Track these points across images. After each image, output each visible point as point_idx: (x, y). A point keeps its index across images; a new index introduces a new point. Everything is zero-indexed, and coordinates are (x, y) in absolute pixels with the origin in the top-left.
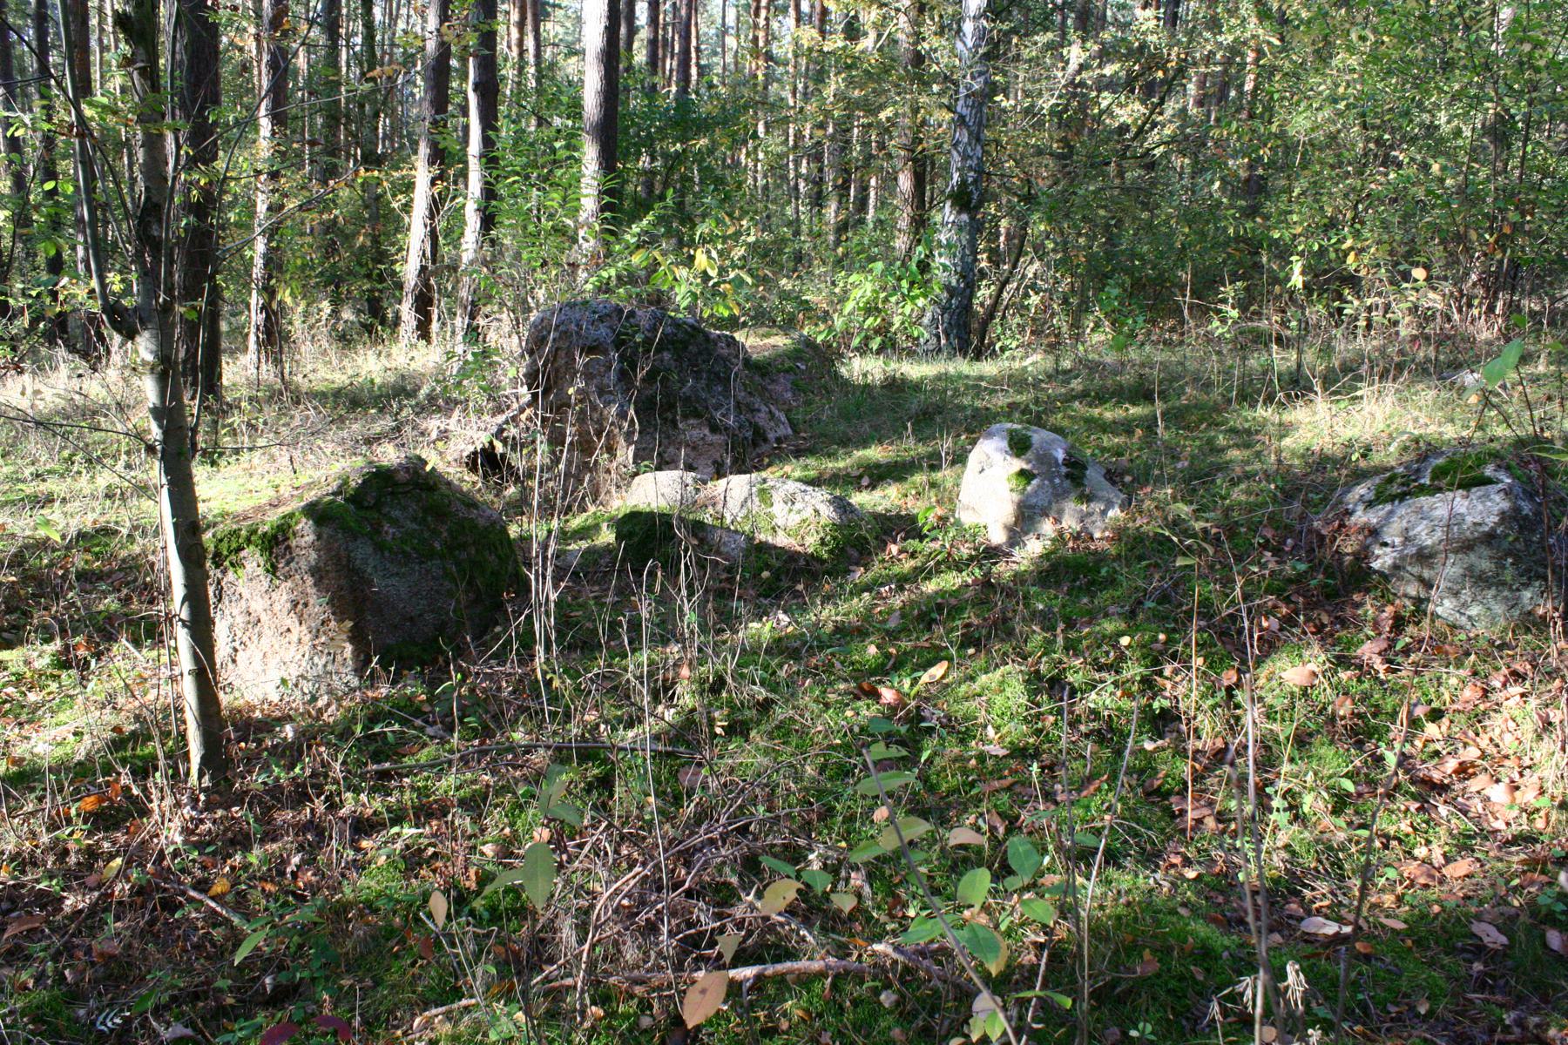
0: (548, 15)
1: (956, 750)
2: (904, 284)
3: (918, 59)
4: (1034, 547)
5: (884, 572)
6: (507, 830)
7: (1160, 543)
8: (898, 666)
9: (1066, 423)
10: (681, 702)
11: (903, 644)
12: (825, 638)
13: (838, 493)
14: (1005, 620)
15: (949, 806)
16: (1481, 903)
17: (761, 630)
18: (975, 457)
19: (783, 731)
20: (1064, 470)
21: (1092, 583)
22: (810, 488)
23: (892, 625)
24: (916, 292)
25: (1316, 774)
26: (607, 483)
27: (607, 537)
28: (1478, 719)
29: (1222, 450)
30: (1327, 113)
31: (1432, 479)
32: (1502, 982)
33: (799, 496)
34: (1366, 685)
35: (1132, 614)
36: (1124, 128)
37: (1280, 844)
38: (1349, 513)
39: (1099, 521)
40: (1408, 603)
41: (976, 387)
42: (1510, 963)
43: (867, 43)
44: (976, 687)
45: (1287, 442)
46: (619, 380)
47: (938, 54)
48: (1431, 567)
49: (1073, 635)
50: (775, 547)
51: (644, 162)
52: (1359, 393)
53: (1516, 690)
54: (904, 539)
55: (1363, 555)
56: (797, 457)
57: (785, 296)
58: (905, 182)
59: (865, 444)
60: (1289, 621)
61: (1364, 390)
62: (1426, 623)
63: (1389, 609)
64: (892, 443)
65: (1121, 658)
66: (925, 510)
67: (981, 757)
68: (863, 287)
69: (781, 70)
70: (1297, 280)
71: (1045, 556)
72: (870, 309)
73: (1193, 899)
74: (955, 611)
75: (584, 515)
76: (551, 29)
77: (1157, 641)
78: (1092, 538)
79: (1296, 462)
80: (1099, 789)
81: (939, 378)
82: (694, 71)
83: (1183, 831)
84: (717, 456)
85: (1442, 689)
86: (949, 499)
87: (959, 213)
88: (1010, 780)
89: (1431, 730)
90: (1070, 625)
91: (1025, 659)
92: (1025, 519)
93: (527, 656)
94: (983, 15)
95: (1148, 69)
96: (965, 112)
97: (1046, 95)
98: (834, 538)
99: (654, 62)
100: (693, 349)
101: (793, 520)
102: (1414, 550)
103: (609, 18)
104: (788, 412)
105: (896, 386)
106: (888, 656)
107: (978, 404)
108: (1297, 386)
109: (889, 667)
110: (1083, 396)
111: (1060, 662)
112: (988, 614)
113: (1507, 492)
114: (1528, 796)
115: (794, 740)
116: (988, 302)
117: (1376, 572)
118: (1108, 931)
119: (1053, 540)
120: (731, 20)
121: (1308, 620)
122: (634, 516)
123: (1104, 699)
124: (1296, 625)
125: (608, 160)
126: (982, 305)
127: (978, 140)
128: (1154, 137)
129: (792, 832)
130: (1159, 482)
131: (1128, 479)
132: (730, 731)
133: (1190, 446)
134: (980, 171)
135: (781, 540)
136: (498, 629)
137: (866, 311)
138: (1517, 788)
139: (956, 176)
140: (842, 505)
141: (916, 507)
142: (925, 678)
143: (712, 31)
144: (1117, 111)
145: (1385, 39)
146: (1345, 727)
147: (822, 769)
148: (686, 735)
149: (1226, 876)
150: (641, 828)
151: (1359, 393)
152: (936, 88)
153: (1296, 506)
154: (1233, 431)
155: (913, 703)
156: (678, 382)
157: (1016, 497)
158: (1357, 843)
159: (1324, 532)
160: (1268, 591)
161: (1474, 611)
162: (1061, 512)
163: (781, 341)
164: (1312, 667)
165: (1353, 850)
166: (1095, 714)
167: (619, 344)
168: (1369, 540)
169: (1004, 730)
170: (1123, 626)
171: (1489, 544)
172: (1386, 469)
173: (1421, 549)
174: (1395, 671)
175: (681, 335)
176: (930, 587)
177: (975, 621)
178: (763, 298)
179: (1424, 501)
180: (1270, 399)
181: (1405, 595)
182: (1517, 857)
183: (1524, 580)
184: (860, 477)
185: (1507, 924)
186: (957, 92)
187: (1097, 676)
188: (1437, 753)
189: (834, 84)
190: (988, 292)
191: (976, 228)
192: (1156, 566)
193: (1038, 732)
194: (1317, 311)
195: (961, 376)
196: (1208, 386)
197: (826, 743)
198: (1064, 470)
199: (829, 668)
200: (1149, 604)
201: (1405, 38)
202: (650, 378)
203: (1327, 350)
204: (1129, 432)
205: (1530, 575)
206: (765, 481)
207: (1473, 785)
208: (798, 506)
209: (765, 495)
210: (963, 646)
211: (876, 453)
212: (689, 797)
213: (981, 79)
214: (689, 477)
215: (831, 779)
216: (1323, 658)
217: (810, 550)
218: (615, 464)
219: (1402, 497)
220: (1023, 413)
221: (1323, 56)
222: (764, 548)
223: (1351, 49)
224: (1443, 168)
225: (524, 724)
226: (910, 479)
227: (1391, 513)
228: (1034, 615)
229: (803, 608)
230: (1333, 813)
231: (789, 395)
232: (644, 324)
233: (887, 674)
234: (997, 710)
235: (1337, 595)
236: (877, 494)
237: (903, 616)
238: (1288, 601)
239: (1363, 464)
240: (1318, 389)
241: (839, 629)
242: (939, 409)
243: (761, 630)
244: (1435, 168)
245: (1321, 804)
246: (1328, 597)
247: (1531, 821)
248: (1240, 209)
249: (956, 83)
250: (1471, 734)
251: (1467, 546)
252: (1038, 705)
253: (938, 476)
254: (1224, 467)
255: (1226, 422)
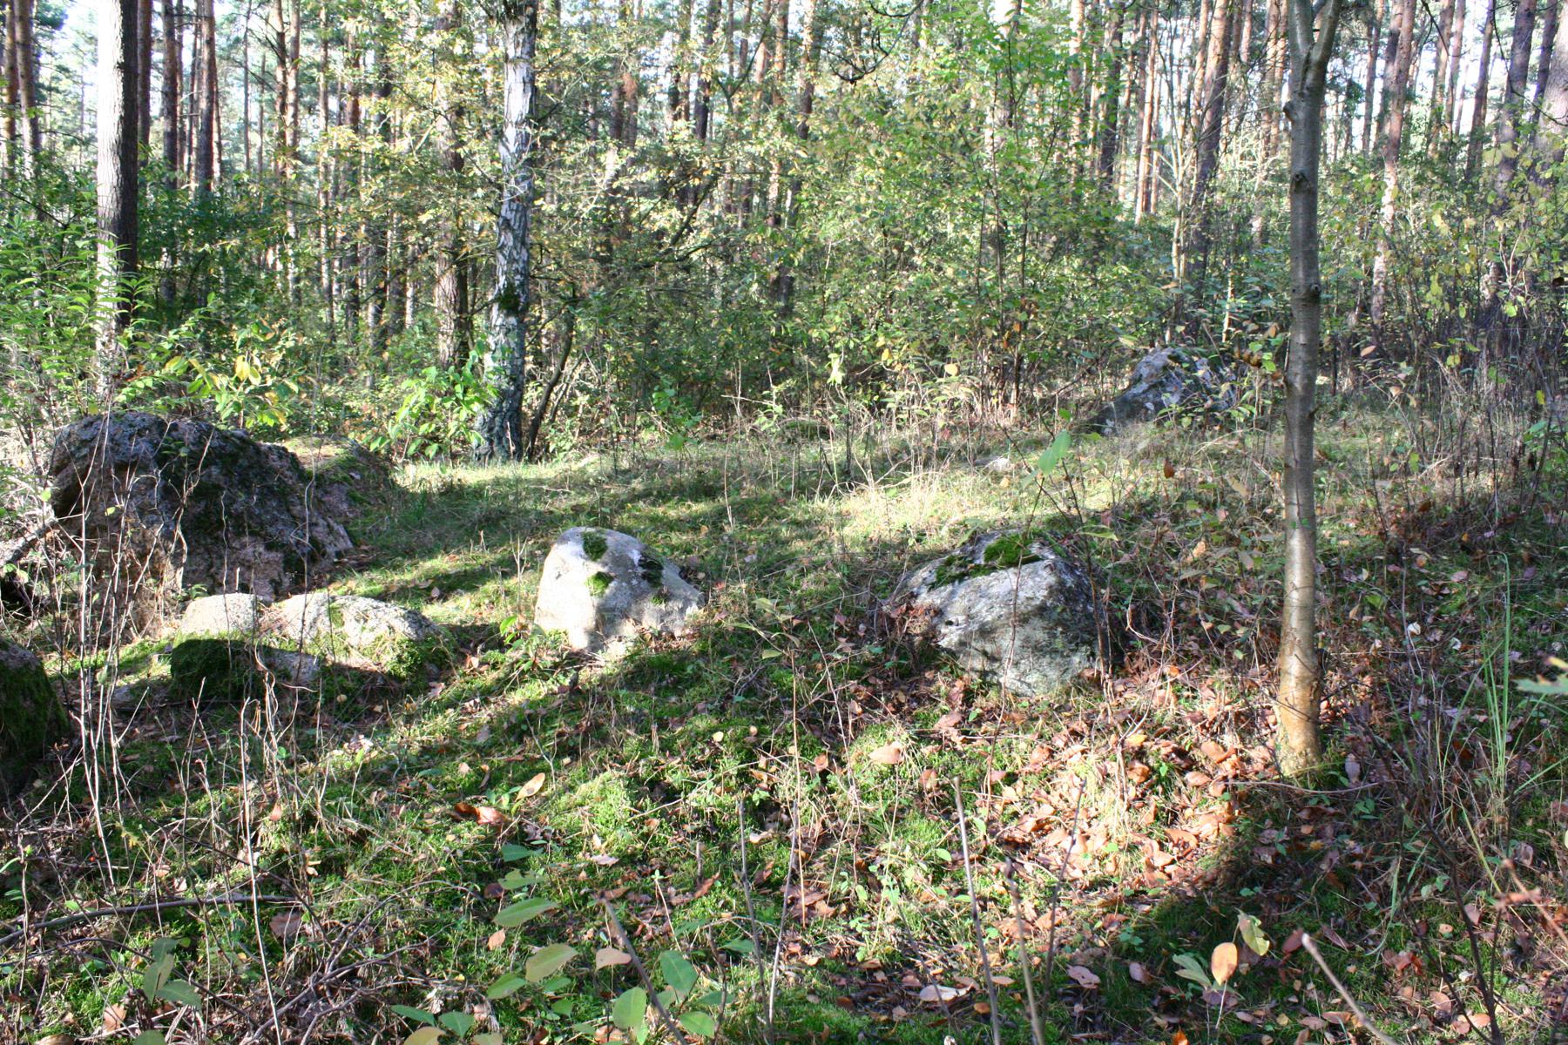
0: (44, 98)
1: (564, 864)
2: (459, 389)
3: (458, 162)
4: (615, 653)
5: (467, 687)
6: (70, 1017)
7: (740, 637)
8: (493, 783)
9: (631, 523)
10: (265, 844)
11: (495, 760)
12: (413, 760)
13: (409, 606)
14: (599, 726)
15: (564, 923)
16: (1073, 948)
17: (336, 759)
18: (552, 562)
19: (382, 863)
20: (640, 571)
21: (678, 681)
22: (382, 604)
23: (481, 740)
24: (470, 396)
25: (913, 848)
26: (155, 609)
27: (160, 669)
28: (1047, 777)
29: (786, 542)
30: (854, 220)
31: (986, 560)
32: (1100, 1018)
33: (371, 613)
34: (947, 758)
35: (723, 709)
36: (662, 233)
37: (889, 919)
38: (914, 596)
39: (677, 620)
40: (975, 676)
41: (538, 489)
42: (1104, 999)
43: (401, 146)
44: (577, 797)
45: (847, 531)
46: (163, 498)
47: (476, 158)
48: (993, 641)
49: (666, 735)
50: (350, 668)
51: (164, 262)
52: (905, 481)
53: (1077, 747)
54: (484, 651)
55: (931, 635)
56: (360, 571)
57: (327, 403)
58: (447, 285)
59: (431, 554)
60: (870, 703)
61: (910, 478)
62: (992, 694)
63: (959, 683)
64: (459, 553)
65: (717, 754)
66: (502, 618)
67: (591, 869)
68: (414, 393)
69: (310, 169)
70: (837, 376)
71: (630, 659)
72: (425, 415)
73: (819, 985)
74: (548, 719)
75: (129, 647)
76: (51, 115)
77: (749, 734)
78: (673, 637)
79: (858, 550)
80: (713, 888)
81: (497, 482)
82: (216, 167)
83: (798, 919)
84: (275, 575)
85: (1014, 754)
86: (526, 607)
87: (507, 315)
88: (623, 889)
89: (1009, 793)
90: (663, 726)
91: (623, 763)
92: (606, 621)
93: (82, 811)
94: (527, 121)
95: (684, 176)
96: (510, 216)
97: (585, 199)
98: (412, 655)
99: (173, 157)
100: (243, 462)
101: (368, 638)
102: (976, 627)
103: (125, 107)
104: (346, 524)
105: (453, 492)
106: (481, 773)
107: (540, 507)
108: (850, 476)
109: (483, 785)
110: (645, 495)
111: (658, 764)
112: (578, 722)
113: (1052, 568)
114: (1097, 843)
115: (395, 872)
116: (536, 403)
117: (944, 650)
118: (745, 1032)
119: (635, 641)
120: (254, 116)
121: (888, 700)
122: (191, 645)
123: (705, 797)
124: (878, 706)
125: (129, 261)
126: (530, 407)
127: (523, 243)
128: (690, 242)
129: (406, 972)
130: (734, 577)
131: (701, 575)
132: (325, 869)
133: (756, 541)
134: (527, 276)
135: (355, 661)
136: (38, 784)
137: (416, 417)
138: (1088, 838)
139: (502, 279)
140: (417, 620)
141: (491, 617)
142: (523, 792)
143: (234, 126)
144: (654, 215)
145: (899, 155)
146: (932, 799)
147: (429, 900)
148: (279, 878)
149: (843, 957)
150: (238, 990)
151: (905, 481)
152: (480, 192)
153: (865, 593)
154: (798, 524)
155: (516, 821)
156: (235, 502)
157: (596, 601)
158: (958, 909)
159: (893, 615)
160: (850, 677)
161: (1033, 678)
162: (640, 613)
163: (332, 451)
164: (897, 745)
165: (956, 915)
166: (699, 813)
167: (161, 460)
168: (936, 620)
169: (610, 839)
170: (715, 722)
171: (1041, 616)
172: (946, 552)
173: (983, 625)
174: (970, 741)
175: (229, 449)
176: (516, 698)
177: (568, 730)
178: (305, 406)
179: (981, 580)
180: (825, 491)
181: (972, 669)
182: (1097, 901)
183: (1073, 646)
184: (429, 589)
185: (1097, 966)
186: (501, 196)
187: (695, 774)
188: (1016, 815)
189: (369, 188)
190: (535, 394)
191: (522, 328)
192: (739, 659)
193: (645, 837)
194: (858, 405)
195: (518, 480)
196: (764, 481)
197: (430, 872)
198: (640, 571)
199: (421, 791)
200: (738, 698)
201: (917, 158)
202: (198, 495)
203: (870, 442)
204: (696, 529)
205: (1076, 642)
206: (334, 599)
207: (1051, 839)
208: (371, 623)
209: (333, 613)
210: (559, 756)
211: (442, 563)
212: (288, 948)
213: (525, 184)
214: (246, 599)
215: (439, 909)
216: (905, 735)
217: (387, 669)
218: (162, 589)
219: (961, 578)
220: (589, 514)
221: (842, 169)
222: (340, 669)
223: (871, 164)
224: (956, 272)
225: (81, 889)
226: (482, 588)
227: (953, 593)
228: (625, 720)
229: (387, 728)
230: (934, 882)
231: (345, 507)
232: (189, 438)
233: (482, 792)
234: (601, 818)
235: (910, 674)
236: (450, 605)
237: (492, 730)
238: (866, 682)
239: (919, 548)
240: (870, 479)
241: (426, 750)
242: (503, 515)
243: (336, 759)
244: (950, 272)
245: (921, 876)
246: (902, 677)
247: (1102, 866)
248: (777, 310)
249: (500, 188)
250: (1043, 793)
251: (1024, 620)
252: (642, 809)
253: (511, 583)
254: (791, 559)
255: (787, 514)
